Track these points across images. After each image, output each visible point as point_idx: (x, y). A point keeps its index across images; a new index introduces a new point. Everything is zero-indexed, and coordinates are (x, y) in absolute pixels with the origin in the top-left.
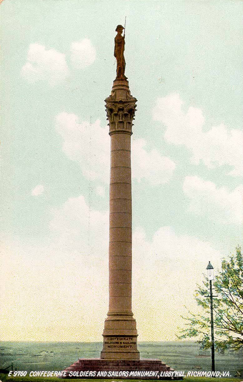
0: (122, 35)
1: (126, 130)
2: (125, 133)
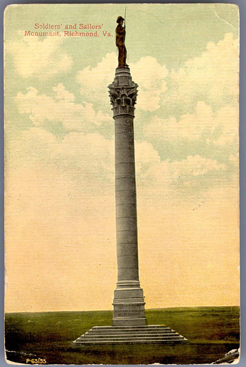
0: (123, 26)
1: (128, 114)
2: (128, 116)
